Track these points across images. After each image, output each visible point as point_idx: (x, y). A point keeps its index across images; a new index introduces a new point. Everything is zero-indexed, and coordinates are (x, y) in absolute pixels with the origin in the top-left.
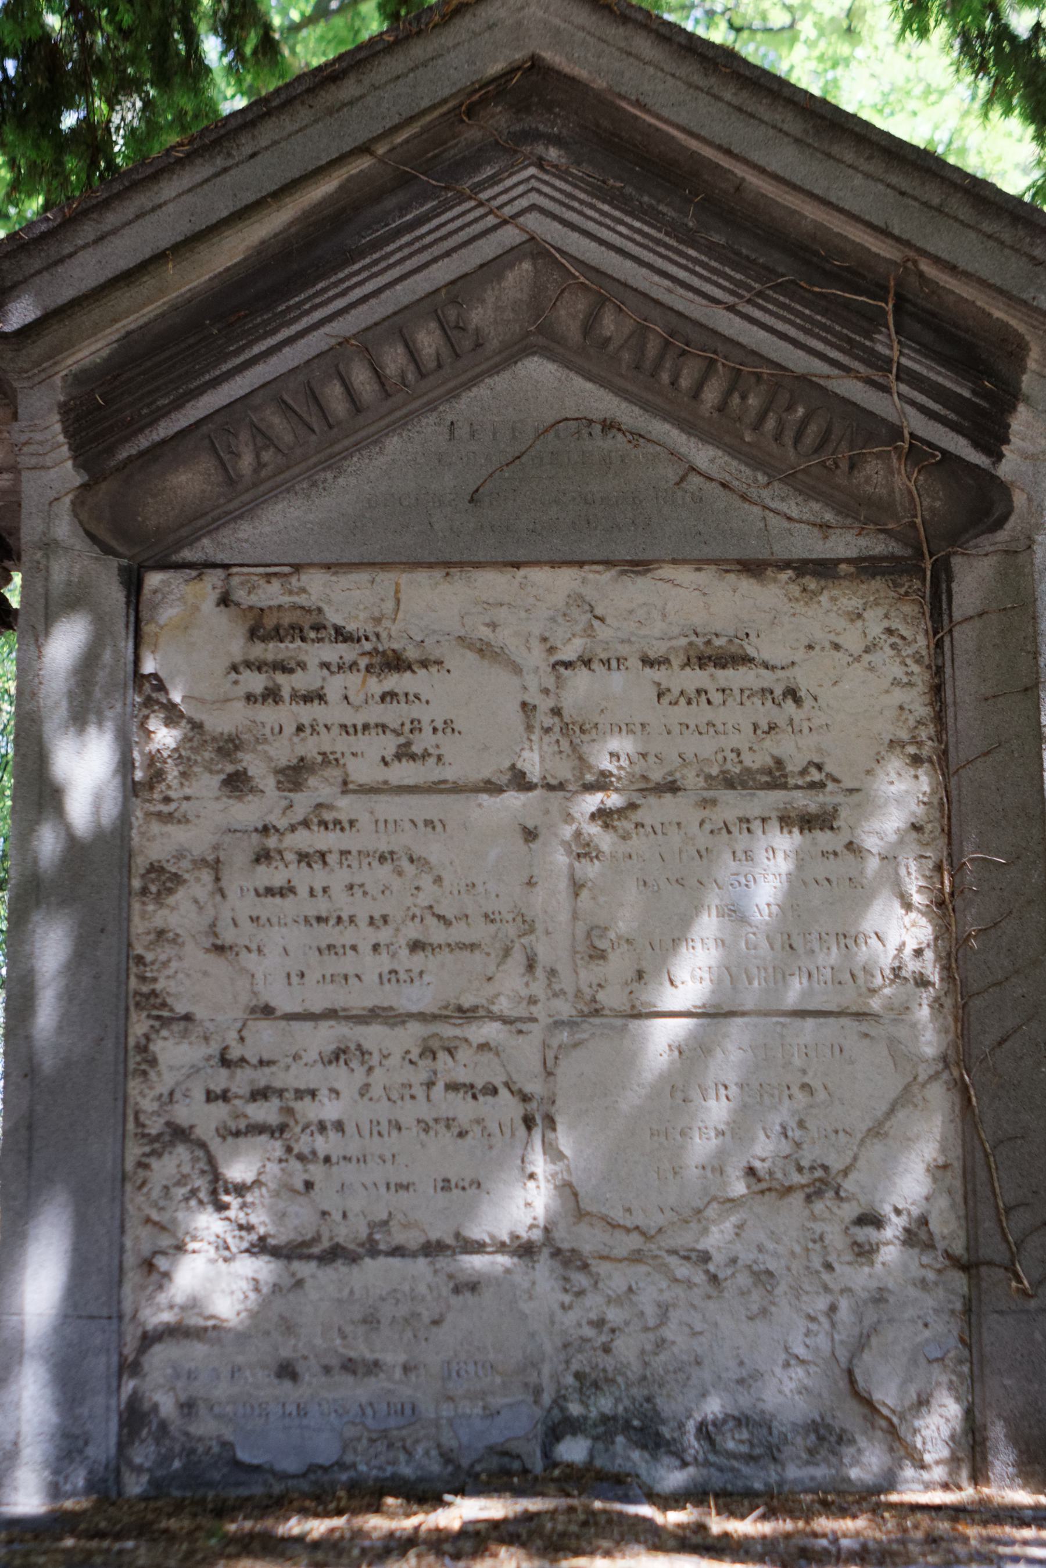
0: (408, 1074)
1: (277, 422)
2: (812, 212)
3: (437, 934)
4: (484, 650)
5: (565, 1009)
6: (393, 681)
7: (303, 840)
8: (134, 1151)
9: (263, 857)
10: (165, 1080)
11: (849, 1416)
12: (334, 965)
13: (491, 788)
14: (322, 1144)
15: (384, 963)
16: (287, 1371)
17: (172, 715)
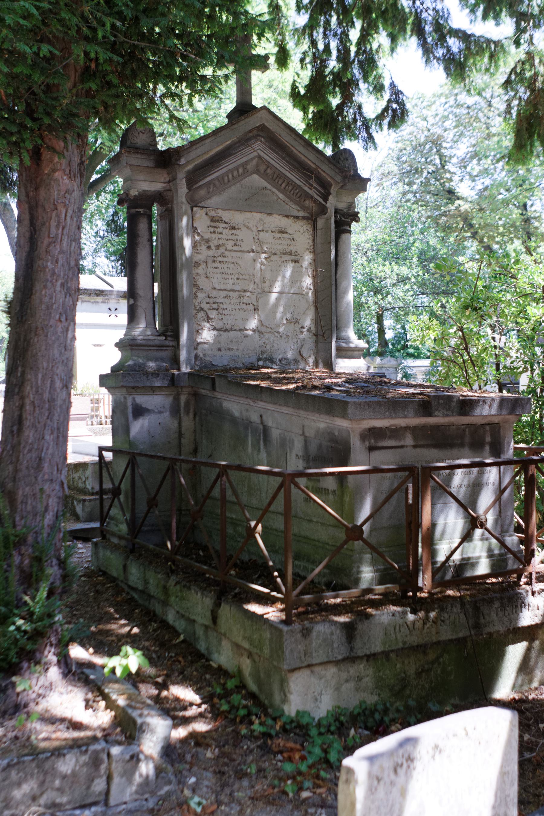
0: (236, 301)
1: (217, 183)
2: (303, 157)
3: (241, 277)
4: (248, 227)
5: (259, 291)
6: (233, 231)
7: (220, 259)
8: (195, 312)
9: (214, 261)
10: (199, 300)
11: (299, 358)
12: (225, 281)
13: (249, 252)
14: (224, 312)
15: (232, 281)
16: (220, 350)
17: (198, 234)
